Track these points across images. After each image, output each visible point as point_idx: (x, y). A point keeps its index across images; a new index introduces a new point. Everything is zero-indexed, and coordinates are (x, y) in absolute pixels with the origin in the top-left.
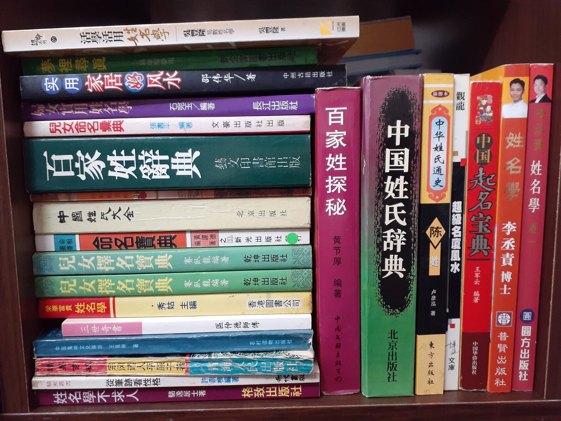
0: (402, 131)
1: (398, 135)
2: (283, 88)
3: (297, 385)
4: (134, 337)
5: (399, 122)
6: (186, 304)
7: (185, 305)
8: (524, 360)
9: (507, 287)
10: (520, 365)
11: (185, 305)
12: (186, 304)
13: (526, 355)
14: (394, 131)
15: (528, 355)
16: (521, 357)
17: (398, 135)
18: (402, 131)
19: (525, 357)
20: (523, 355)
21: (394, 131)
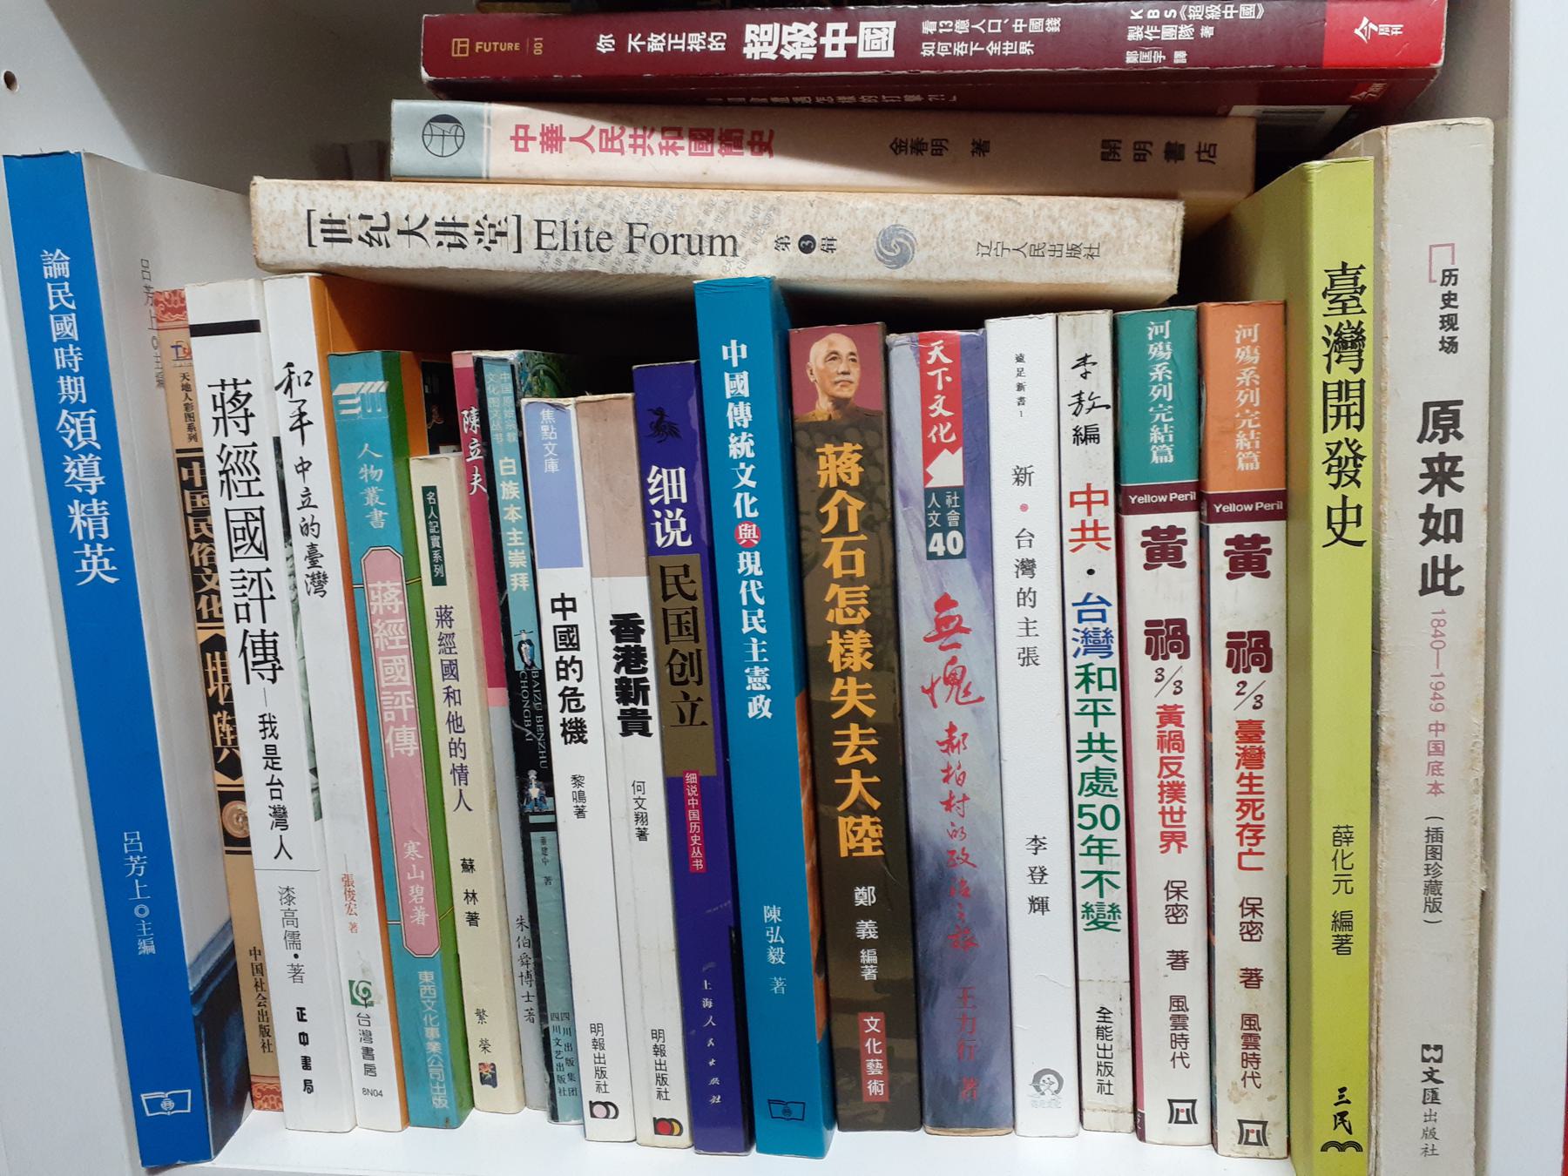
0: (739, 352)
5: (734, 343)
18: (739, 352)
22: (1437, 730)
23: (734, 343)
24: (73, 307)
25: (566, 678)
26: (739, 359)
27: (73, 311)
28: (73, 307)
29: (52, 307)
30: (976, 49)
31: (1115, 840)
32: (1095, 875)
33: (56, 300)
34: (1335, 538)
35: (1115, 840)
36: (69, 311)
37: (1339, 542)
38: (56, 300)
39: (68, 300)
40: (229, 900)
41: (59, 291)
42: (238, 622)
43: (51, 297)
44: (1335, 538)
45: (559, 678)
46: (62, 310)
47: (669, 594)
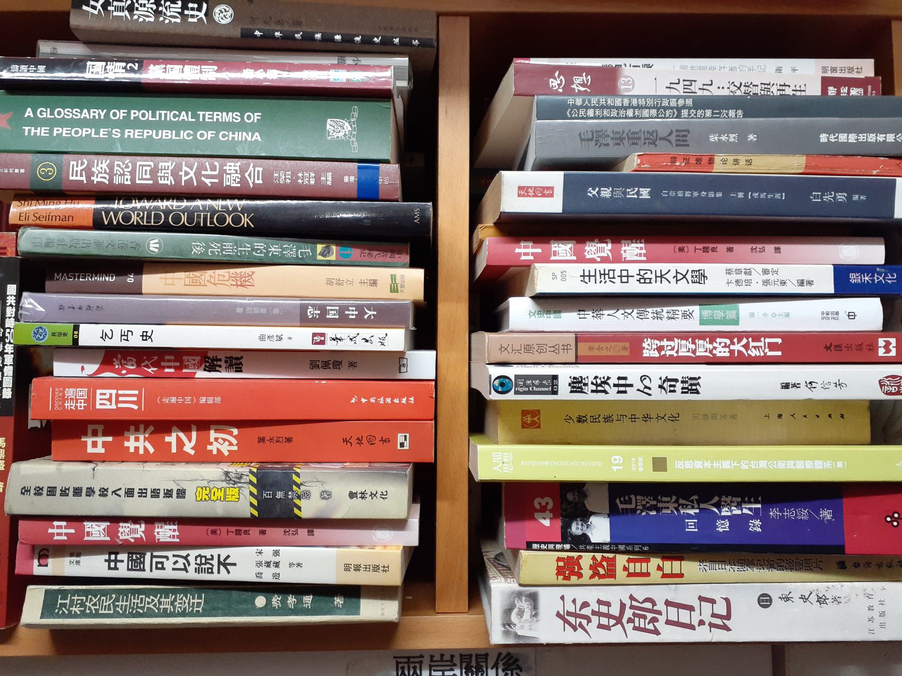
0: (352, 315)
1: (351, 313)
2: (784, 248)
3: (593, 261)
4: (175, 57)
5: (357, 313)
6: (592, 273)
7: (589, 276)
8: (867, 138)
9: (373, 315)
10: (872, 140)
11: (589, 276)
12: (592, 273)
13: (864, 136)
14: (353, 310)
15: (864, 134)
16: (865, 140)
17: (351, 313)
18: (352, 315)
19: (865, 138)
20: (864, 139)
21: (353, 310)
22: (628, 276)
23: (357, 313)
24: (636, 189)
25: (650, 279)
26: (349, 315)
27: (638, 189)
28: (636, 189)
29: (636, 196)
30: (735, 465)
31: (595, 270)
32: (221, 567)
33: (633, 194)
34: (684, 279)
35: (595, 270)
36: (638, 191)
37: (687, 276)
38: (633, 194)
39: (634, 190)
40: (626, 634)
41: (630, 193)
42: (206, 286)
43: (632, 196)
44: (684, 279)
45: (650, 283)
46: (638, 193)
47: (183, 567)
